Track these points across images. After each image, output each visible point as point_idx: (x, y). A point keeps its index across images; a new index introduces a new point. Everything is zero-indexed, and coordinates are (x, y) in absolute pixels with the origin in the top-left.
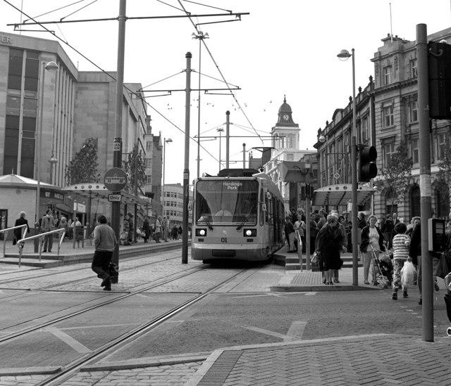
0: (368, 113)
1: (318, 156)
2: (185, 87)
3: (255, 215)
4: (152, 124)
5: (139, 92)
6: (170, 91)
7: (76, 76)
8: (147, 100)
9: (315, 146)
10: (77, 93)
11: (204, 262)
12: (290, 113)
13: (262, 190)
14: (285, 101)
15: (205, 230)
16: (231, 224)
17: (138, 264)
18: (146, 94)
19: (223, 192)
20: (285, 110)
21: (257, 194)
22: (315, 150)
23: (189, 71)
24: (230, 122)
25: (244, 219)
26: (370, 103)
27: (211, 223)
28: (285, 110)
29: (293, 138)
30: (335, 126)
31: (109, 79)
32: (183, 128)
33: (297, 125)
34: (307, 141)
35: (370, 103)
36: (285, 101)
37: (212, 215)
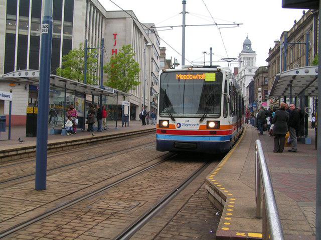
0: (311, 29)
1: (269, 67)
2: (181, 24)
3: (218, 107)
4: (166, 52)
5: (152, 29)
6: (172, 27)
7: (105, 14)
8: (160, 34)
9: (268, 60)
10: (106, 25)
11: (170, 152)
12: (250, 45)
13: (226, 81)
14: (247, 37)
15: (168, 121)
16: (194, 115)
17: (104, 151)
18: (157, 29)
19: (169, 84)
20: (247, 44)
21: (221, 85)
22: (267, 64)
23: (184, 13)
24: (212, 53)
25: (207, 111)
26: (313, 20)
27: (174, 115)
28: (247, 44)
29: (251, 60)
30: (304, 22)
31: (127, 16)
32: (181, 54)
33: (255, 52)
34: (261, 61)
35: (313, 20)
36: (247, 37)
37: (173, 107)
